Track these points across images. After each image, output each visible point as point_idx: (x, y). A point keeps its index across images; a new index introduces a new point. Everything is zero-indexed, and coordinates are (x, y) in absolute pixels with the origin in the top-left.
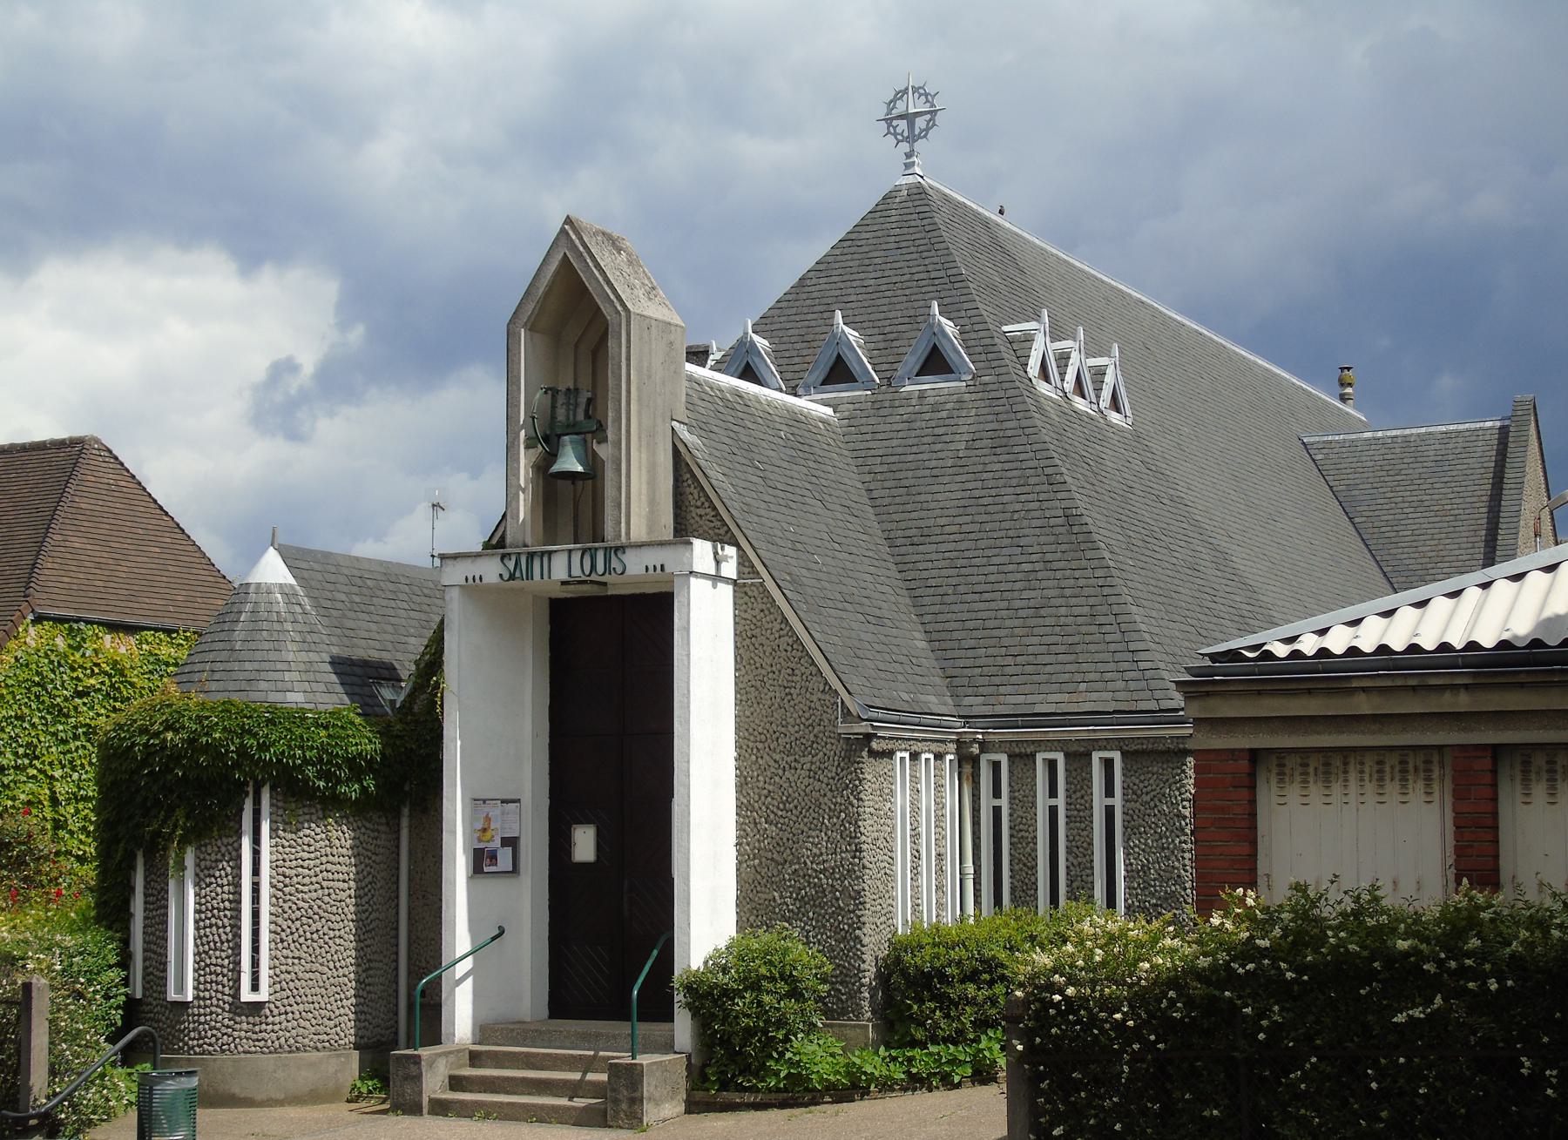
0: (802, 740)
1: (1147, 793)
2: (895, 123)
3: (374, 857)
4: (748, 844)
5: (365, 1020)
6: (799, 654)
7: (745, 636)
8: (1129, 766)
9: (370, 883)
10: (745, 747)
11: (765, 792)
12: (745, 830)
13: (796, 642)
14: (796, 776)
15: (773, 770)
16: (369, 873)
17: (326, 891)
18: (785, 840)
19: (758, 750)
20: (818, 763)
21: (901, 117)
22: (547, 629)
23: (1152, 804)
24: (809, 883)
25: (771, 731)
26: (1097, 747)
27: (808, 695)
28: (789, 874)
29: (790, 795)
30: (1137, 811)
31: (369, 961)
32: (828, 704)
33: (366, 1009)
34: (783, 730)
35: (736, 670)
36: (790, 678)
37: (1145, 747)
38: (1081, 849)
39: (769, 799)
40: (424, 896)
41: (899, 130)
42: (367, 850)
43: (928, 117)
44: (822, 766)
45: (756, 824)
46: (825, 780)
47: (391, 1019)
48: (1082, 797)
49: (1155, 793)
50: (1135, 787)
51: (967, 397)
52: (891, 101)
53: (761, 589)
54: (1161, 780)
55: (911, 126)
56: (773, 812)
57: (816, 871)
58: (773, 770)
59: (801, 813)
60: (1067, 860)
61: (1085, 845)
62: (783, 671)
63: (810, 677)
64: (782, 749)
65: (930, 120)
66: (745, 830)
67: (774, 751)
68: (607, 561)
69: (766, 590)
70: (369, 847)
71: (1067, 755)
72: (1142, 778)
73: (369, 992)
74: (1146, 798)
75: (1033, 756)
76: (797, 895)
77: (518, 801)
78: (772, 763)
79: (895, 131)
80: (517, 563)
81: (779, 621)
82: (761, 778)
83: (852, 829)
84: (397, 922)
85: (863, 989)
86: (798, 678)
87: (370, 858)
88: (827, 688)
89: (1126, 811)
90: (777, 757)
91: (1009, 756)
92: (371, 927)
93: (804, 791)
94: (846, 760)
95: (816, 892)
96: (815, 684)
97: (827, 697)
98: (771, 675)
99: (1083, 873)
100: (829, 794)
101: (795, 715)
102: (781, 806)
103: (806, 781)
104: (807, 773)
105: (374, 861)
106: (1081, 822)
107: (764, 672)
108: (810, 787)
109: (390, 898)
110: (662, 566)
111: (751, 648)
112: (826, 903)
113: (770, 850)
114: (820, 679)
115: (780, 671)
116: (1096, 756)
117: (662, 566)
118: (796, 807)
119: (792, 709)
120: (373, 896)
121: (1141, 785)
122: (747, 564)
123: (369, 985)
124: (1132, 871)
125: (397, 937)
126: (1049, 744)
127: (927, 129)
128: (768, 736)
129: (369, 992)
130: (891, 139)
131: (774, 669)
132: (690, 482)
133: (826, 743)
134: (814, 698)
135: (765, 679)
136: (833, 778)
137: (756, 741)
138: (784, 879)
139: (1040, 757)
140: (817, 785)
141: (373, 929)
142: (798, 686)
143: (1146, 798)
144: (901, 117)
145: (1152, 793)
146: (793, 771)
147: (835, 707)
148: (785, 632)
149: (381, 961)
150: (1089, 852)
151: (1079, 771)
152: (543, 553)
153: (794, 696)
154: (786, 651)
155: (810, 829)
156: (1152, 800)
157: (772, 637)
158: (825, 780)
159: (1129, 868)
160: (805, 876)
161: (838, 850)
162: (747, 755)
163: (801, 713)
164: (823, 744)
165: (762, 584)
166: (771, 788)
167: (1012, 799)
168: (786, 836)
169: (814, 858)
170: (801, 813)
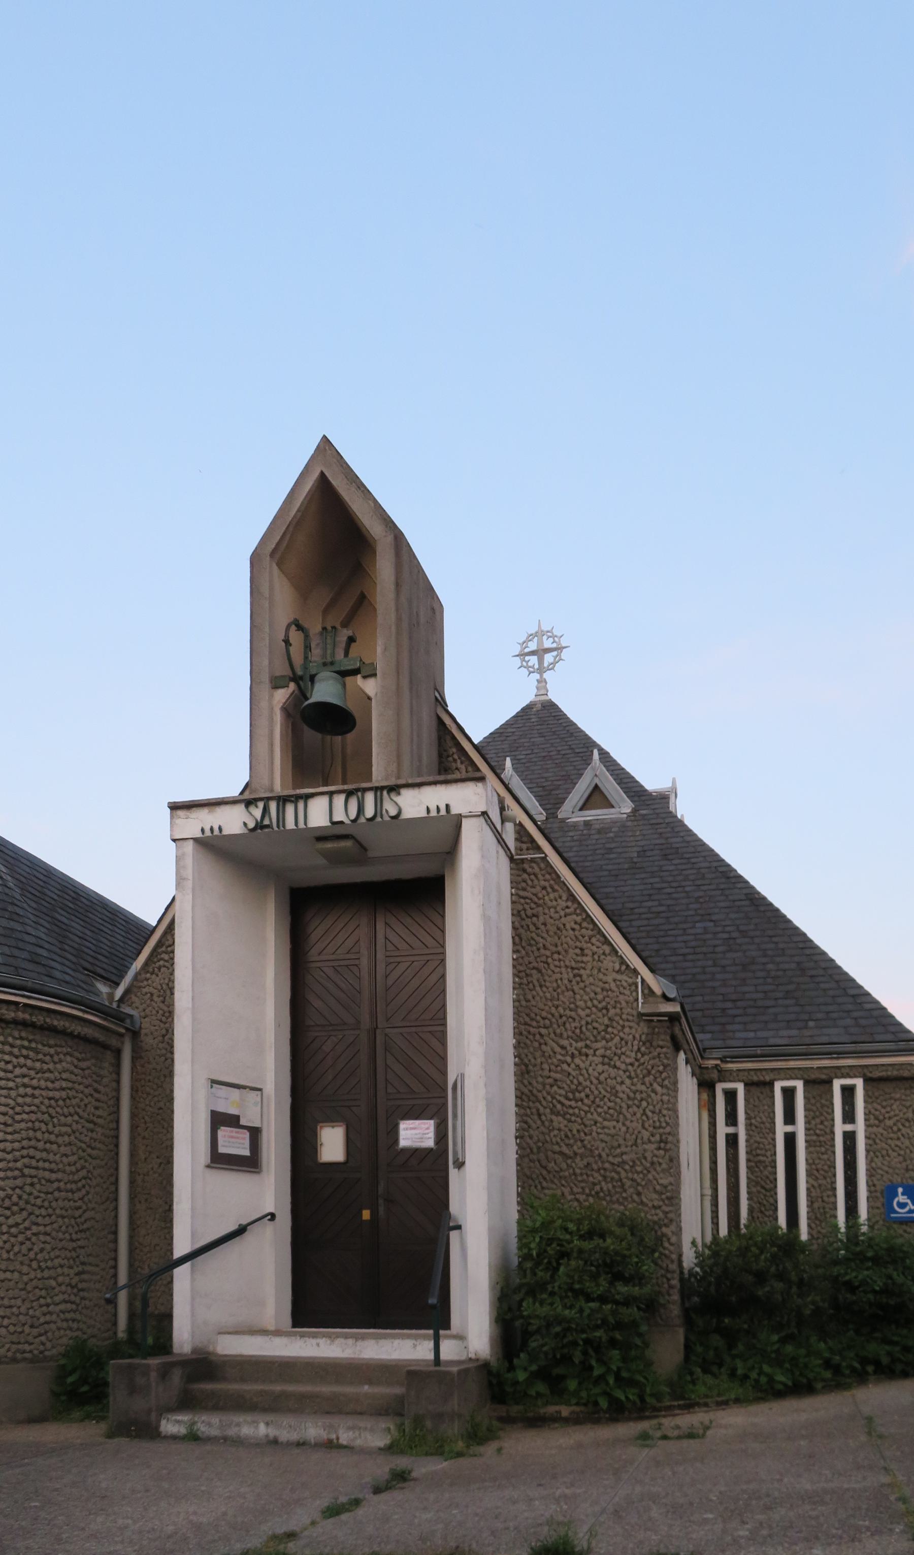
0: (595, 1025)
1: (890, 1118)
2: (527, 658)
3: (89, 1150)
4: (531, 1137)
5: (78, 1329)
6: (590, 933)
7: (524, 916)
8: (870, 1093)
9: (85, 1178)
10: (525, 1033)
11: (550, 1081)
12: (526, 1122)
13: (584, 920)
14: (588, 1063)
15: (559, 1057)
16: (83, 1168)
17: (29, 1180)
18: (575, 1132)
19: (541, 1035)
20: (614, 1048)
21: (533, 653)
22: (289, 918)
23: (895, 1128)
24: (605, 1177)
25: (557, 1014)
26: (839, 1074)
27: (601, 976)
28: (580, 1168)
29: (580, 1084)
30: (879, 1136)
31: (83, 1263)
32: (625, 984)
33: (78, 1316)
34: (573, 1014)
35: (514, 952)
36: (579, 958)
37: (889, 1073)
38: (822, 1172)
39: (555, 1088)
40: (146, 1200)
41: (530, 664)
42: (81, 1141)
43: (555, 653)
44: (619, 1052)
45: (539, 1115)
46: (623, 1067)
47: (108, 1330)
48: (822, 1123)
49: (897, 1118)
50: (877, 1113)
51: (629, 824)
52: (524, 642)
53: (542, 865)
54: (904, 1106)
55: (541, 661)
56: (559, 1102)
57: (613, 1164)
58: (559, 1057)
59: (593, 1102)
60: (807, 1182)
61: (826, 1168)
62: (571, 951)
63: (602, 957)
64: (570, 1033)
65: (557, 656)
66: (526, 1122)
67: (561, 1035)
68: (379, 803)
69: (549, 865)
70: (83, 1137)
71: (807, 1083)
72: (884, 1104)
73: (83, 1298)
74: (889, 1123)
75: (771, 1084)
76: (590, 1191)
77: (260, 1090)
78: (558, 1049)
79: (527, 664)
80: (266, 810)
81: (564, 898)
82: (546, 1066)
83: (656, 1119)
84: (116, 1225)
85: (671, 1292)
86: (589, 958)
87: (84, 1151)
88: (624, 967)
89: (868, 1135)
90: (565, 1043)
91: (746, 1085)
92: (85, 1226)
93: (598, 1079)
94: (648, 1044)
95: (614, 1187)
96: (610, 963)
97: (624, 977)
98: (556, 956)
99: (825, 1194)
100: (628, 1082)
101: (586, 998)
102: (570, 1095)
103: (600, 1068)
104: (600, 1059)
105: (89, 1155)
106: (821, 1146)
107: (548, 953)
108: (605, 1075)
109: (108, 1199)
110: (447, 806)
111: (532, 928)
112: (625, 1199)
113: (557, 1143)
114: (614, 958)
115: (566, 951)
116: (837, 1084)
117: (447, 806)
118: (587, 1096)
119: (582, 992)
120: (88, 1193)
121: (883, 1111)
122: (525, 839)
123: (82, 1290)
124: (876, 1191)
125: (116, 1241)
126: (789, 1072)
127: (554, 664)
128: (554, 1020)
129: (83, 1298)
130: (525, 671)
131: (560, 948)
132: (456, 757)
133: (623, 1027)
134: (609, 979)
135: (550, 960)
136: (632, 1064)
137: (539, 1027)
138: (575, 1174)
139: (778, 1086)
140: (613, 1072)
141: (88, 1229)
142: (589, 966)
143: (889, 1123)
144: (533, 653)
145: (896, 1118)
146: (584, 1058)
147: (633, 988)
148: (572, 910)
149: (97, 1266)
150: (830, 1174)
151: (818, 1098)
152: (298, 798)
153: (585, 977)
154: (573, 930)
155: (605, 1119)
156: (895, 1124)
157: (557, 916)
158: (623, 1067)
159: (873, 1188)
160: (599, 1170)
161: (639, 1141)
162: (528, 1042)
163: (592, 995)
164: (619, 1028)
165: (544, 859)
166: (558, 1076)
167: (749, 1126)
168: (575, 1127)
169: (610, 1150)
170: (593, 1102)
